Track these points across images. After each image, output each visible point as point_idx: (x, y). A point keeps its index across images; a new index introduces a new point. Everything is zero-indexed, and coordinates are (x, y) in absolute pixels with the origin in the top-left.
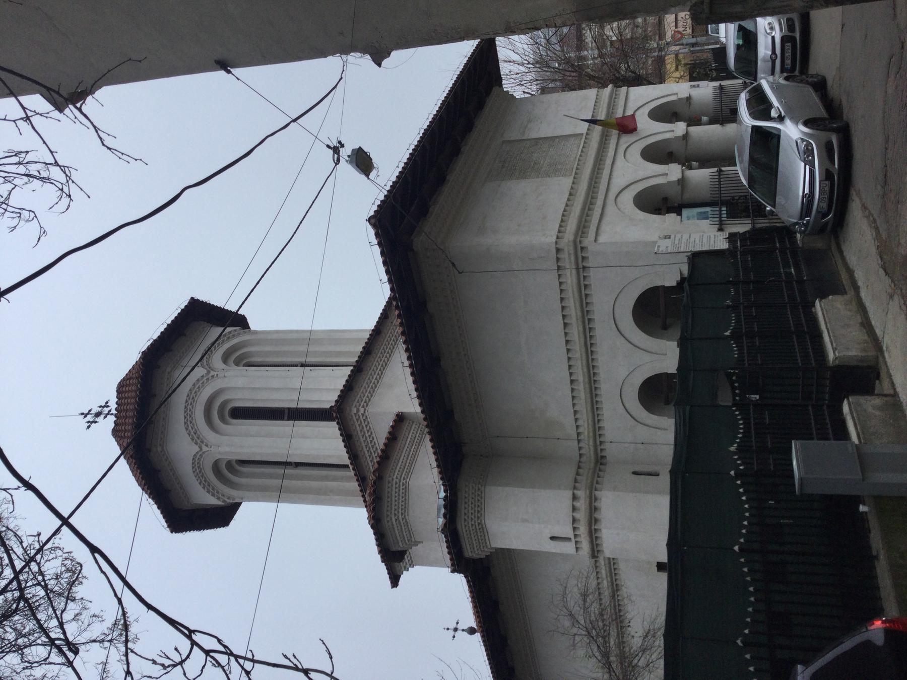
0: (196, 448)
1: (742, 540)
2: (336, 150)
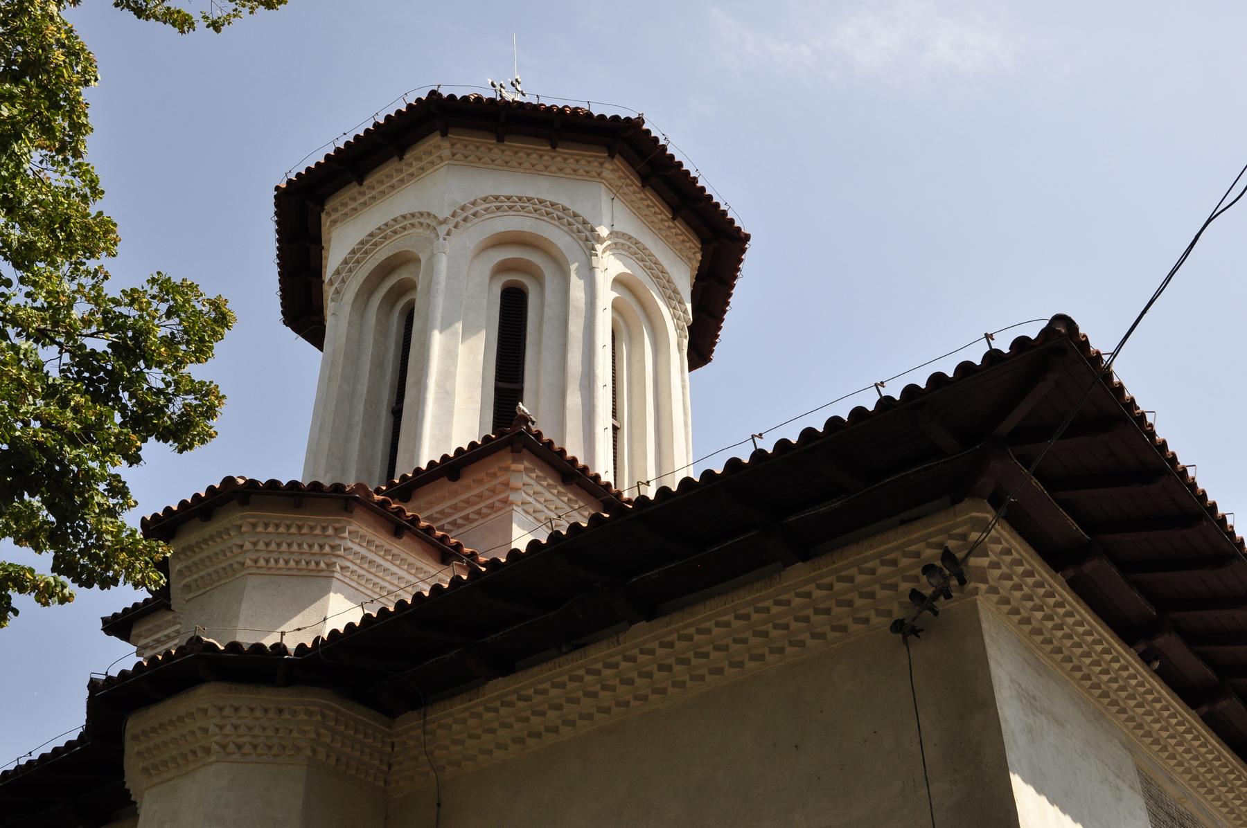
0: (447, 213)
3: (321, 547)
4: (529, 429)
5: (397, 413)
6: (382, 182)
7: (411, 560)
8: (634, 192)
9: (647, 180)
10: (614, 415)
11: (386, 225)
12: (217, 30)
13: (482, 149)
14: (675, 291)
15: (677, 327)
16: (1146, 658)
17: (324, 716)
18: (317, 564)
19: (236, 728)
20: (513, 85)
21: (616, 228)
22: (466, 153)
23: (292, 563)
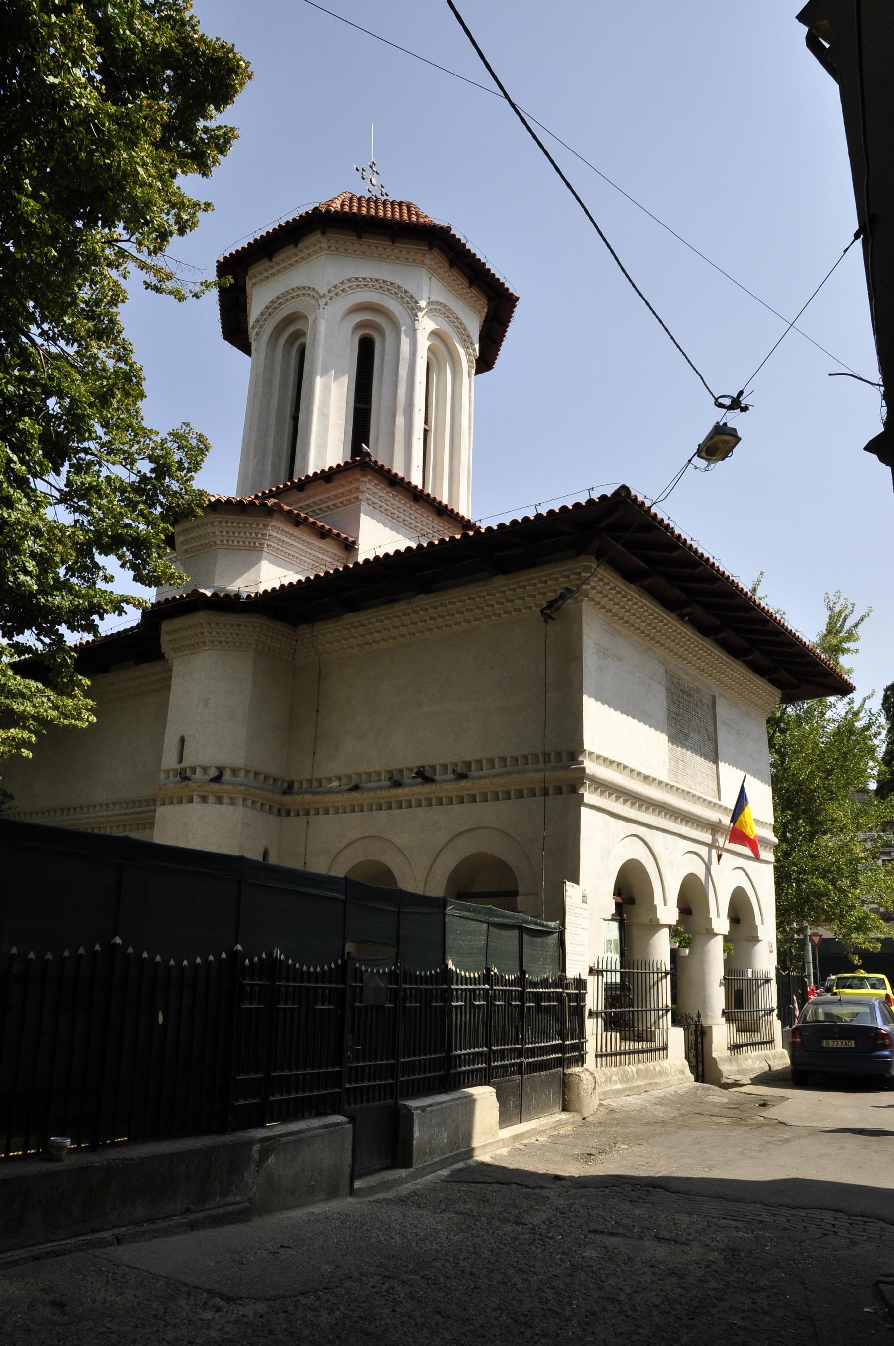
1: (130, 950)
2: (736, 404)
3: (256, 534)
4: (370, 460)
5: (295, 419)
6: (284, 261)
7: (304, 538)
8: (445, 272)
9: (452, 263)
10: (426, 422)
11: (287, 292)
12: (198, 298)
13: (348, 243)
14: (469, 336)
15: (469, 361)
16: (681, 617)
17: (261, 628)
18: (255, 543)
19: (218, 633)
20: (371, 167)
21: (431, 300)
22: (338, 246)
23: (241, 543)
